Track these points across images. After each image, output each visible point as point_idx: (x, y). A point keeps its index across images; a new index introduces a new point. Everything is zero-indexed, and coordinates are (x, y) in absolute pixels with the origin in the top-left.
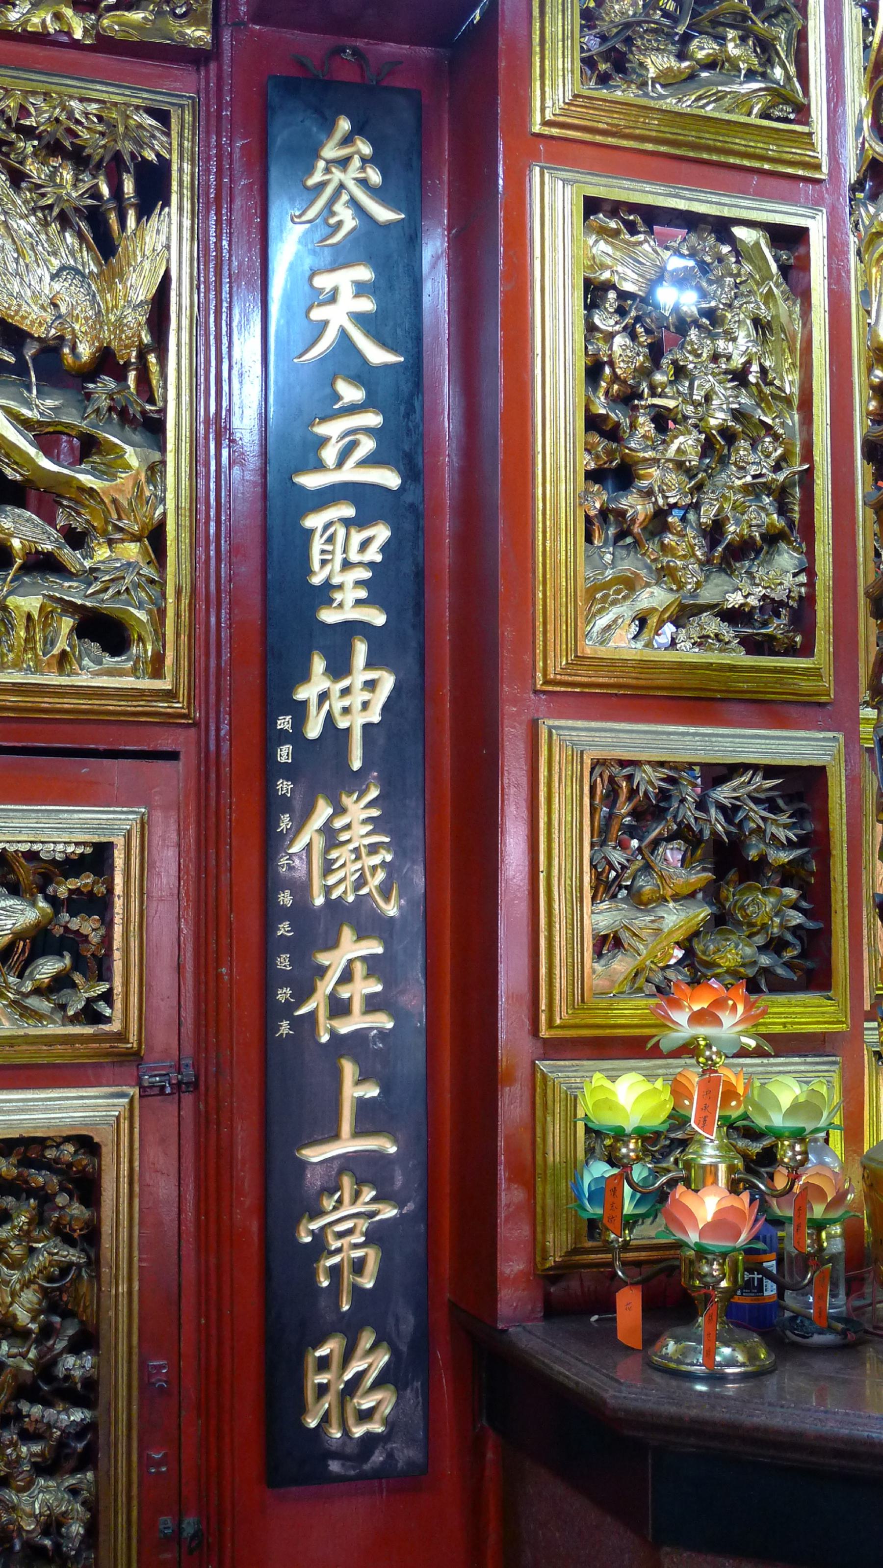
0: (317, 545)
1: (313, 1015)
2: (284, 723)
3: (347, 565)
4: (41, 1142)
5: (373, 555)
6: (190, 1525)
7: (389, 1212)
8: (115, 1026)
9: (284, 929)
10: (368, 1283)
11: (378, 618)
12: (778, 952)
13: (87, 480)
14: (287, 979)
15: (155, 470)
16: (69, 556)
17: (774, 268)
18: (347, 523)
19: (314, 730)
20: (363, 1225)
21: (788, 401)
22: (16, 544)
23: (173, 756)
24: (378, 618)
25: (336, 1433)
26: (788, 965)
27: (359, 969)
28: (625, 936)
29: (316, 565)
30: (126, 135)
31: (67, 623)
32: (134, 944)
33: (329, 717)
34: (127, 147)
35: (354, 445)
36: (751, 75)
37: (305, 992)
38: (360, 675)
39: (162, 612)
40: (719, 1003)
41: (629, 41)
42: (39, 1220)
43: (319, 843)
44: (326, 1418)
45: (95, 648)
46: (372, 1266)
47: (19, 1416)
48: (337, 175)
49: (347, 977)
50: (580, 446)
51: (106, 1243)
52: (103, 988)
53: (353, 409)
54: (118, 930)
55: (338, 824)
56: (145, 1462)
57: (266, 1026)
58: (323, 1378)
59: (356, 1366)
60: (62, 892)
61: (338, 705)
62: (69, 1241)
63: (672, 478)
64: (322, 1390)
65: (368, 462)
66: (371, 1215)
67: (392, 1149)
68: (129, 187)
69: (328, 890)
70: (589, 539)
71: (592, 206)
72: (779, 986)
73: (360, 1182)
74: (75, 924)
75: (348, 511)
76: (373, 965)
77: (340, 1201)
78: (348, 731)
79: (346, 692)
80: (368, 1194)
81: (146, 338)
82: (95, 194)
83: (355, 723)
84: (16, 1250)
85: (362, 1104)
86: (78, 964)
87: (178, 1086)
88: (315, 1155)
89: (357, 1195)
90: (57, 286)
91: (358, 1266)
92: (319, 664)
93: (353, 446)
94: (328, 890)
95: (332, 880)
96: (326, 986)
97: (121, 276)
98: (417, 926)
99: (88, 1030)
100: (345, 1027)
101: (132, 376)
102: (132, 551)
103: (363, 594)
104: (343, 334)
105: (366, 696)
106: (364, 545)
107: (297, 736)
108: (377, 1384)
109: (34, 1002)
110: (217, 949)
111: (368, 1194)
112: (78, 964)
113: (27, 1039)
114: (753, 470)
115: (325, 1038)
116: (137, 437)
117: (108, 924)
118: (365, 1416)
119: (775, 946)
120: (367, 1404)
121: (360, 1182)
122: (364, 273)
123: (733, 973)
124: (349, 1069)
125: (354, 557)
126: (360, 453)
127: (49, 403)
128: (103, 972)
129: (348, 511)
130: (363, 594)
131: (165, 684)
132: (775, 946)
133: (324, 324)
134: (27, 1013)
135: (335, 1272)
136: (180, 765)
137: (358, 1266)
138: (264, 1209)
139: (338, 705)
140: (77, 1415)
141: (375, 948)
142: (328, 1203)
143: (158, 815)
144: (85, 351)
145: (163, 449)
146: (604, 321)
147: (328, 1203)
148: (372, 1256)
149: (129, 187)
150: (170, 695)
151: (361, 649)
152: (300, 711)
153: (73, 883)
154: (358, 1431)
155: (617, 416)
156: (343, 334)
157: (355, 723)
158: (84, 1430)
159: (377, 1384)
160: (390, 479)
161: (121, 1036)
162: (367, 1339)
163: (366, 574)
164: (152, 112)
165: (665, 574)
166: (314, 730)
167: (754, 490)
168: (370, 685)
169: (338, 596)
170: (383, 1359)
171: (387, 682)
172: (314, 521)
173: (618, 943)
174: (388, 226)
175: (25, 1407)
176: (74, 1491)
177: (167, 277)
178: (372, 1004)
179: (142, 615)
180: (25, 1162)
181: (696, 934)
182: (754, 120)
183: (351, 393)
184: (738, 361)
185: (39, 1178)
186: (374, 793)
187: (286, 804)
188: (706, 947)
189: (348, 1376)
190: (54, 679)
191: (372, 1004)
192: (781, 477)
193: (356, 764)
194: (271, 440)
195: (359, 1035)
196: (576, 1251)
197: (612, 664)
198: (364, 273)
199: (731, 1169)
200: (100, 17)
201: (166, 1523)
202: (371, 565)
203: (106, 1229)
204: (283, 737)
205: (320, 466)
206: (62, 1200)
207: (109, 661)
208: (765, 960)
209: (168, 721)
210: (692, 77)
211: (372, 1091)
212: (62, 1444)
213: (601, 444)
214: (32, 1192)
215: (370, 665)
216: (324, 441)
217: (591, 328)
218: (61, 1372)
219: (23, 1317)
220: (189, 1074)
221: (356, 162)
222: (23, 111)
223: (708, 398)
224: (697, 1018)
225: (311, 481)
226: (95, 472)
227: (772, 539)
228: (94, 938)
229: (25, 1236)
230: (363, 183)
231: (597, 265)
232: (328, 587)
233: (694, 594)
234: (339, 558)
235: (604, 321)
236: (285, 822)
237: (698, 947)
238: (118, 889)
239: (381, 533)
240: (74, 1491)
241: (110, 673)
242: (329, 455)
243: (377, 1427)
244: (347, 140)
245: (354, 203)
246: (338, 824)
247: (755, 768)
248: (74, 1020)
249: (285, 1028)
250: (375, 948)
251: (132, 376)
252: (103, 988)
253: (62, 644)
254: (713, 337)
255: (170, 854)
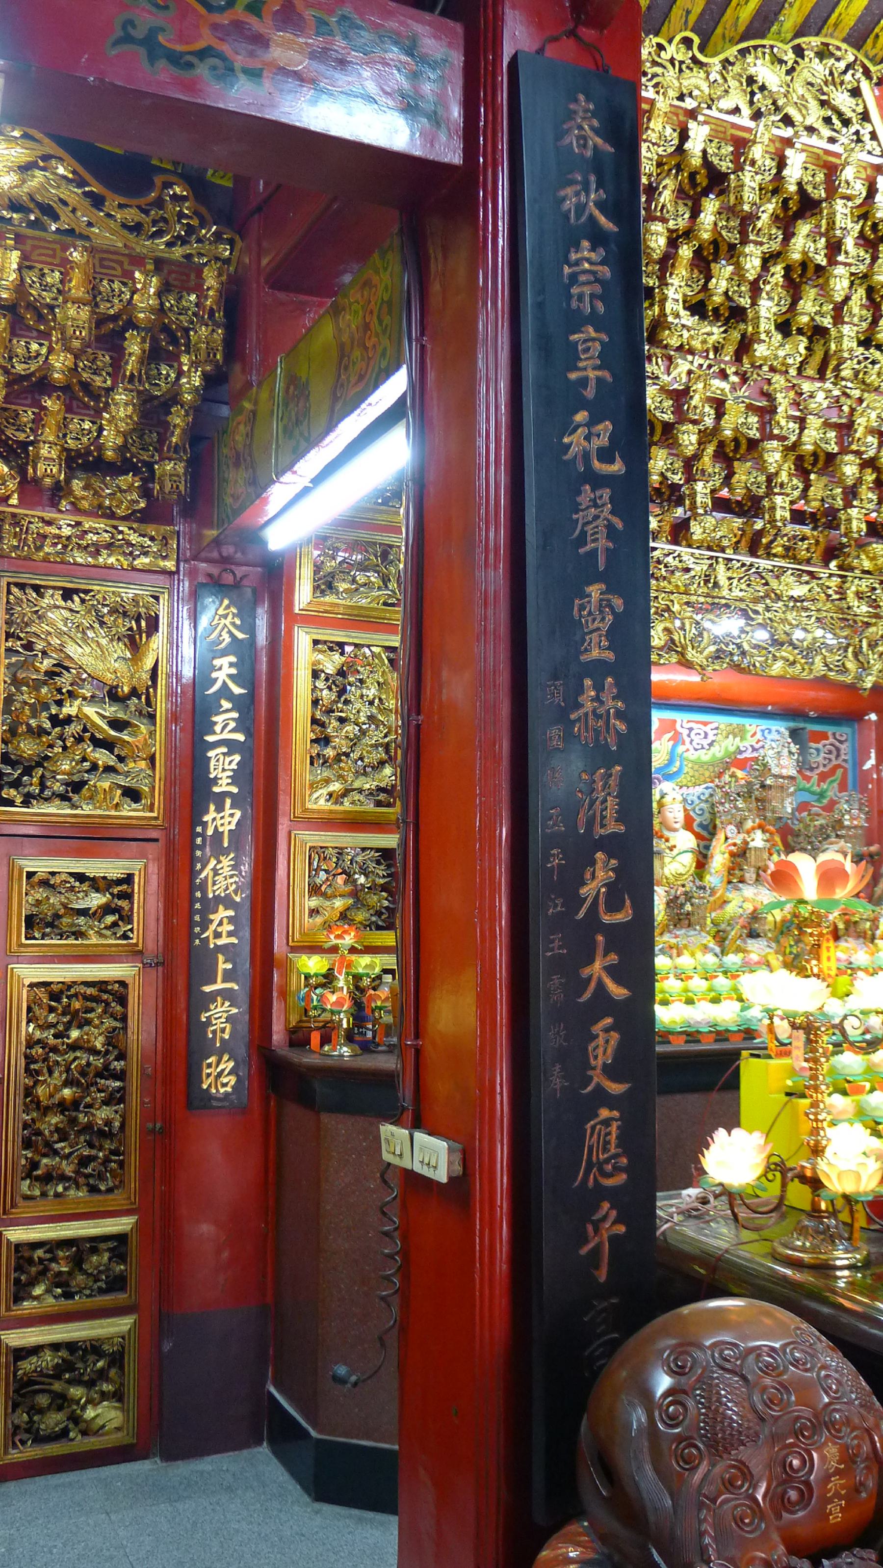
0: (213, 763)
1: (208, 937)
2: (199, 829)
3: (224, 770)
4: (106, 983)
5: (234, 766)
6: (158, 1125)
7: (235, 1011)
8: (134, 941)
9: (198, 906)
10: (227, 1037)
11: (235, 790)
12: (380, 917)
13: (126, 738)
14: (198, 924)
15: (152, 734)
16: (120, 766)
17: (386, 661)
18: (224, 754)
19: (210, 832)
20: (225, 1015)
21: (391, 710)
22: (100, 763)
23: (156, 840)
24: (235, 790)
25: (214, 1091)
26: (383, 921)
27: (225, 921)
28: (321, 909)
29: (212, 770)
30: (143, 606)
31: (119, 792)
32: (141, 910)
33: (216, 826)
34: (142, 610)
35: (227, 724)
36: (379, 588)
37: (205, 929)
38: (228, 811)
39: (154, 787)
40: (345, 932)
41: (333, 577)
42: (105, 1012)
43: (211, 874)
44: (210, 1086)
45: (128, 800)
46: (228, 1030)
47: (96, 1083)
48: (223, 621)
49: (220, 924)
50: (309, 729)
51: (129, 1021)
52: (130, 927)
53: (227, 711)
54: (136, 905)
55: (218, 867)
56: (143, 1103)
57: (191, 936)
58: (209, 1071)
59: (221, 1067)
60: (116, 891)
61: (219, 822)
62: (116, 1019)
63: (343, 742)
64: (209, 1075)
65: (233, 731)
66: (227, 1011)
67: (236, 987)
68: (143, 624)
69: (214, 892)
70: (312, 763)
71: (316, 642)
72: (379, 928)
73: (224, 999)
74: (120, 903)
75: (225, 750)
76: (231, 920)
77: (216, 1006)
78: (223, 833)
79: (222, 818)
80: (227, 1004)
81: (150, 683)
82: (131, 629)
83: (225, 829)
84: (96, 1022)
85: (225, 970)
86: (121, 918)
87: (157, 964)
88: (207, 989)
89: (223, 1004)
90: (117, 665)
91: (223, 1030)
92: (212, 807)
93: (226, 725)
94: (214, 892)
95: (215, 888)
96: (213, 927)
97: (141, 660)
98: (248, 904)
99: (125, 942)
100: (220, 942)
101: (143, 697)
102: (143, 764)
103: (230, 781)
104: (224, 682)
105: (230, 819)
106: (230, 763)
107: (203, 835)
108: (229, 1074)
109: (104, 932)
110: (336, 387)
111: (227, 1004)
112: (121, 918)
113: (103, 945)
114: (375, 738)
115: (212, 946)
116: (145, 721)
117: (132, 903)
118: (224, 1085)
119: (379, 914)
120: (225, 1080)
121: (224, 999)
122: (233, 659)
123: (360, 923)
124: (221, 958)
125: (226, 767)
126: (229, 728)
127: (113, 709)
128: (130, 921)
129: (225, 750)
130: (230, 781)
131: (155, 814)
132: (379, 914)
133: (216, 680)
134: (102, 935)
135: (214, 1032)
136: (159, 844)
137: (223, 1030)
138: (188, 1009)
139: (219, 822)
140: (118, 1084)
141: (231, 913)
142: (212, 1007)
143: (150, 865)
144: (126, 689)
145: (155, 725)
146: (320, 684)
147: (212, 1007)
148: (228, 1026)
149: (143, 624)
150: (156, 818)
151: (228, 802)
152: (205, 825)
153: (119, 888)
154: (222, 1090)
155: (324, 719)
156: (224, 682)
157: (225, 829)
158: (119, 1089)
159: (229, 1074)
160: (241, 737)
161: (136, 945)
162: (226, 1057)
163: (231, 774)
164: (152, 596)
165: (340, 777)
166: (210, 832)
167: (376, 746)
168: (232, 815)
169: (220, 782)
170: (231, 1064)
171: (238, 814)
172: (211, 754)
173: (318, 912)
174: (242, 641)
175: (98, 1080)
176: (116, 1112)
177: (157, 661)
178: (230, 934)
179: (146, 789)
180: (101, 990)
181: (348, 909)
182: (380, 606)
183: (226, 705)
184: (371, 697)
185: (105, 996)
186: (232, 855)
187: (200, 860)
188: (350, 914)
189: (219, 1070)
190: (113, 813)
191: (230, 934)
192: (386, 740)
193: (226, 845)
194: (197, 699)
195: (226, 946)
196: (301, 1021)
197: (319, 811)
198: (233, 659)
199: (348, 988)
200: (134, 559)
201: (150, 1126)
202: (233, 770)
203: (130, 1014)
204: (199, 835)
205: (214, 733)
206: (113, 1004)
207: (134, 806)
208: (374, 919)
209: (155, 827)
210: (357, 590)
211: (229, 966)
212: (111, 1094)
213: (318, 729)
214: (102, 1001)
215: (232, 807)
216: (215, 723)
217: (314, 689)
218: (112, 1067)
219: (99, 1046)
220: (161, 959)
221: (230, 616)
222: (105, 599)
223: (358, 712)
224: (338, 937)
225: (210, 738)
226: (130, 734)
227: (382, 763)
228: (127, 908)
229: (100, 1017)
230: (233, 624)
231: (318, 662)
232: (216, 778)
233: (351, 784)
234: (221, 767)
235: (320, 684)
236: (199, 866)
237: (348, 914)
238: (136, 890)
239: (237, 758)
240: (116, 1112)
241: (134, 810)
242: (218, 728)
243: (229, 1089)
244: (228, 607)
245: (230, 632)
246: (218, 867)
247: (372, 849)
248: (119, 938)
249: (197, 942)
250: (231, 913)
251: (143, 697)
252: (130, 927)
253: (116, 800)
254: (361, 688)
255: (155, 877)
